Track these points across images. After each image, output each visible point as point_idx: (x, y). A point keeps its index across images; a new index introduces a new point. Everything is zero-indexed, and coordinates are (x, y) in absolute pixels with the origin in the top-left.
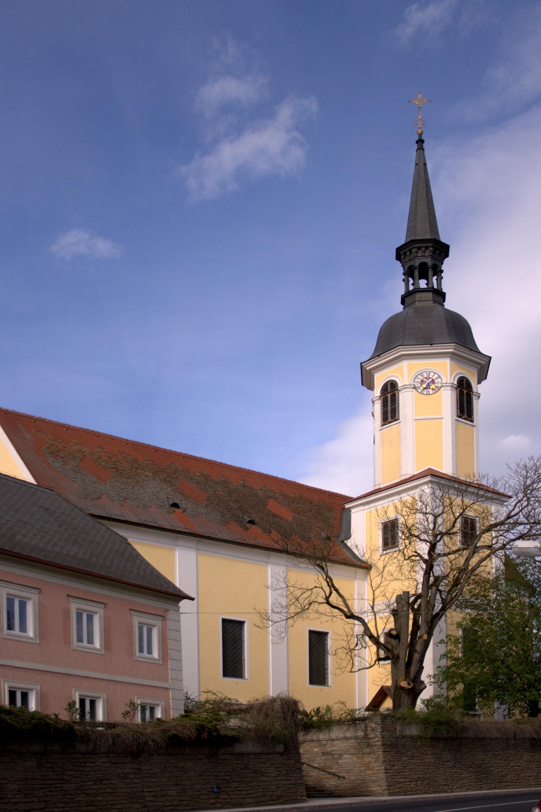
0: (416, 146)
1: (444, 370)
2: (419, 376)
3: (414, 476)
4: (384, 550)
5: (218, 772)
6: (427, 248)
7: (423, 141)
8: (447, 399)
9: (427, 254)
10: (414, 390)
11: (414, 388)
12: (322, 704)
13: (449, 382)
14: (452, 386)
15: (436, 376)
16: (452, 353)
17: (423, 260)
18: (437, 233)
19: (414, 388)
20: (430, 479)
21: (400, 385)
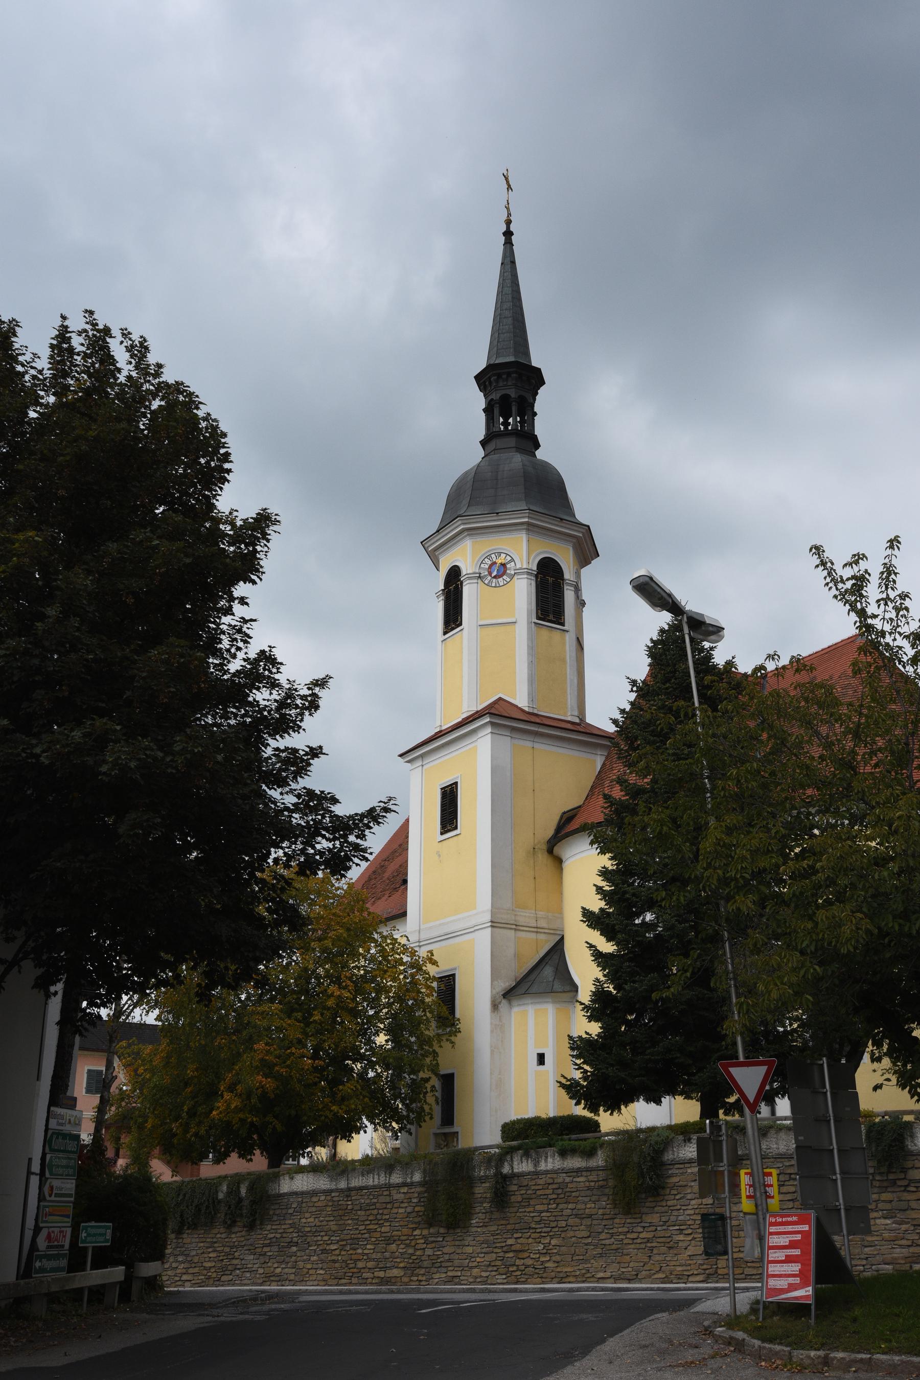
0: (502, 239)
1: (521, 551)
2: (493, 556)
3: (477, 712)
4: (442, 834)
5: (332, 1191)
6: (509, 374)
7: (512, 234)
8: (521, 593)
9: (510, 383)
10: (479, 581)
11: (480, 577)
12: (591, 931)
13: (525, 566)
14: (528, 573)
15: (509, 558)
16: (528, 524)
17: (504, 392)
18: (527, 354)
19: (480, 577)
20: (488, 720)
21: (464, 572)
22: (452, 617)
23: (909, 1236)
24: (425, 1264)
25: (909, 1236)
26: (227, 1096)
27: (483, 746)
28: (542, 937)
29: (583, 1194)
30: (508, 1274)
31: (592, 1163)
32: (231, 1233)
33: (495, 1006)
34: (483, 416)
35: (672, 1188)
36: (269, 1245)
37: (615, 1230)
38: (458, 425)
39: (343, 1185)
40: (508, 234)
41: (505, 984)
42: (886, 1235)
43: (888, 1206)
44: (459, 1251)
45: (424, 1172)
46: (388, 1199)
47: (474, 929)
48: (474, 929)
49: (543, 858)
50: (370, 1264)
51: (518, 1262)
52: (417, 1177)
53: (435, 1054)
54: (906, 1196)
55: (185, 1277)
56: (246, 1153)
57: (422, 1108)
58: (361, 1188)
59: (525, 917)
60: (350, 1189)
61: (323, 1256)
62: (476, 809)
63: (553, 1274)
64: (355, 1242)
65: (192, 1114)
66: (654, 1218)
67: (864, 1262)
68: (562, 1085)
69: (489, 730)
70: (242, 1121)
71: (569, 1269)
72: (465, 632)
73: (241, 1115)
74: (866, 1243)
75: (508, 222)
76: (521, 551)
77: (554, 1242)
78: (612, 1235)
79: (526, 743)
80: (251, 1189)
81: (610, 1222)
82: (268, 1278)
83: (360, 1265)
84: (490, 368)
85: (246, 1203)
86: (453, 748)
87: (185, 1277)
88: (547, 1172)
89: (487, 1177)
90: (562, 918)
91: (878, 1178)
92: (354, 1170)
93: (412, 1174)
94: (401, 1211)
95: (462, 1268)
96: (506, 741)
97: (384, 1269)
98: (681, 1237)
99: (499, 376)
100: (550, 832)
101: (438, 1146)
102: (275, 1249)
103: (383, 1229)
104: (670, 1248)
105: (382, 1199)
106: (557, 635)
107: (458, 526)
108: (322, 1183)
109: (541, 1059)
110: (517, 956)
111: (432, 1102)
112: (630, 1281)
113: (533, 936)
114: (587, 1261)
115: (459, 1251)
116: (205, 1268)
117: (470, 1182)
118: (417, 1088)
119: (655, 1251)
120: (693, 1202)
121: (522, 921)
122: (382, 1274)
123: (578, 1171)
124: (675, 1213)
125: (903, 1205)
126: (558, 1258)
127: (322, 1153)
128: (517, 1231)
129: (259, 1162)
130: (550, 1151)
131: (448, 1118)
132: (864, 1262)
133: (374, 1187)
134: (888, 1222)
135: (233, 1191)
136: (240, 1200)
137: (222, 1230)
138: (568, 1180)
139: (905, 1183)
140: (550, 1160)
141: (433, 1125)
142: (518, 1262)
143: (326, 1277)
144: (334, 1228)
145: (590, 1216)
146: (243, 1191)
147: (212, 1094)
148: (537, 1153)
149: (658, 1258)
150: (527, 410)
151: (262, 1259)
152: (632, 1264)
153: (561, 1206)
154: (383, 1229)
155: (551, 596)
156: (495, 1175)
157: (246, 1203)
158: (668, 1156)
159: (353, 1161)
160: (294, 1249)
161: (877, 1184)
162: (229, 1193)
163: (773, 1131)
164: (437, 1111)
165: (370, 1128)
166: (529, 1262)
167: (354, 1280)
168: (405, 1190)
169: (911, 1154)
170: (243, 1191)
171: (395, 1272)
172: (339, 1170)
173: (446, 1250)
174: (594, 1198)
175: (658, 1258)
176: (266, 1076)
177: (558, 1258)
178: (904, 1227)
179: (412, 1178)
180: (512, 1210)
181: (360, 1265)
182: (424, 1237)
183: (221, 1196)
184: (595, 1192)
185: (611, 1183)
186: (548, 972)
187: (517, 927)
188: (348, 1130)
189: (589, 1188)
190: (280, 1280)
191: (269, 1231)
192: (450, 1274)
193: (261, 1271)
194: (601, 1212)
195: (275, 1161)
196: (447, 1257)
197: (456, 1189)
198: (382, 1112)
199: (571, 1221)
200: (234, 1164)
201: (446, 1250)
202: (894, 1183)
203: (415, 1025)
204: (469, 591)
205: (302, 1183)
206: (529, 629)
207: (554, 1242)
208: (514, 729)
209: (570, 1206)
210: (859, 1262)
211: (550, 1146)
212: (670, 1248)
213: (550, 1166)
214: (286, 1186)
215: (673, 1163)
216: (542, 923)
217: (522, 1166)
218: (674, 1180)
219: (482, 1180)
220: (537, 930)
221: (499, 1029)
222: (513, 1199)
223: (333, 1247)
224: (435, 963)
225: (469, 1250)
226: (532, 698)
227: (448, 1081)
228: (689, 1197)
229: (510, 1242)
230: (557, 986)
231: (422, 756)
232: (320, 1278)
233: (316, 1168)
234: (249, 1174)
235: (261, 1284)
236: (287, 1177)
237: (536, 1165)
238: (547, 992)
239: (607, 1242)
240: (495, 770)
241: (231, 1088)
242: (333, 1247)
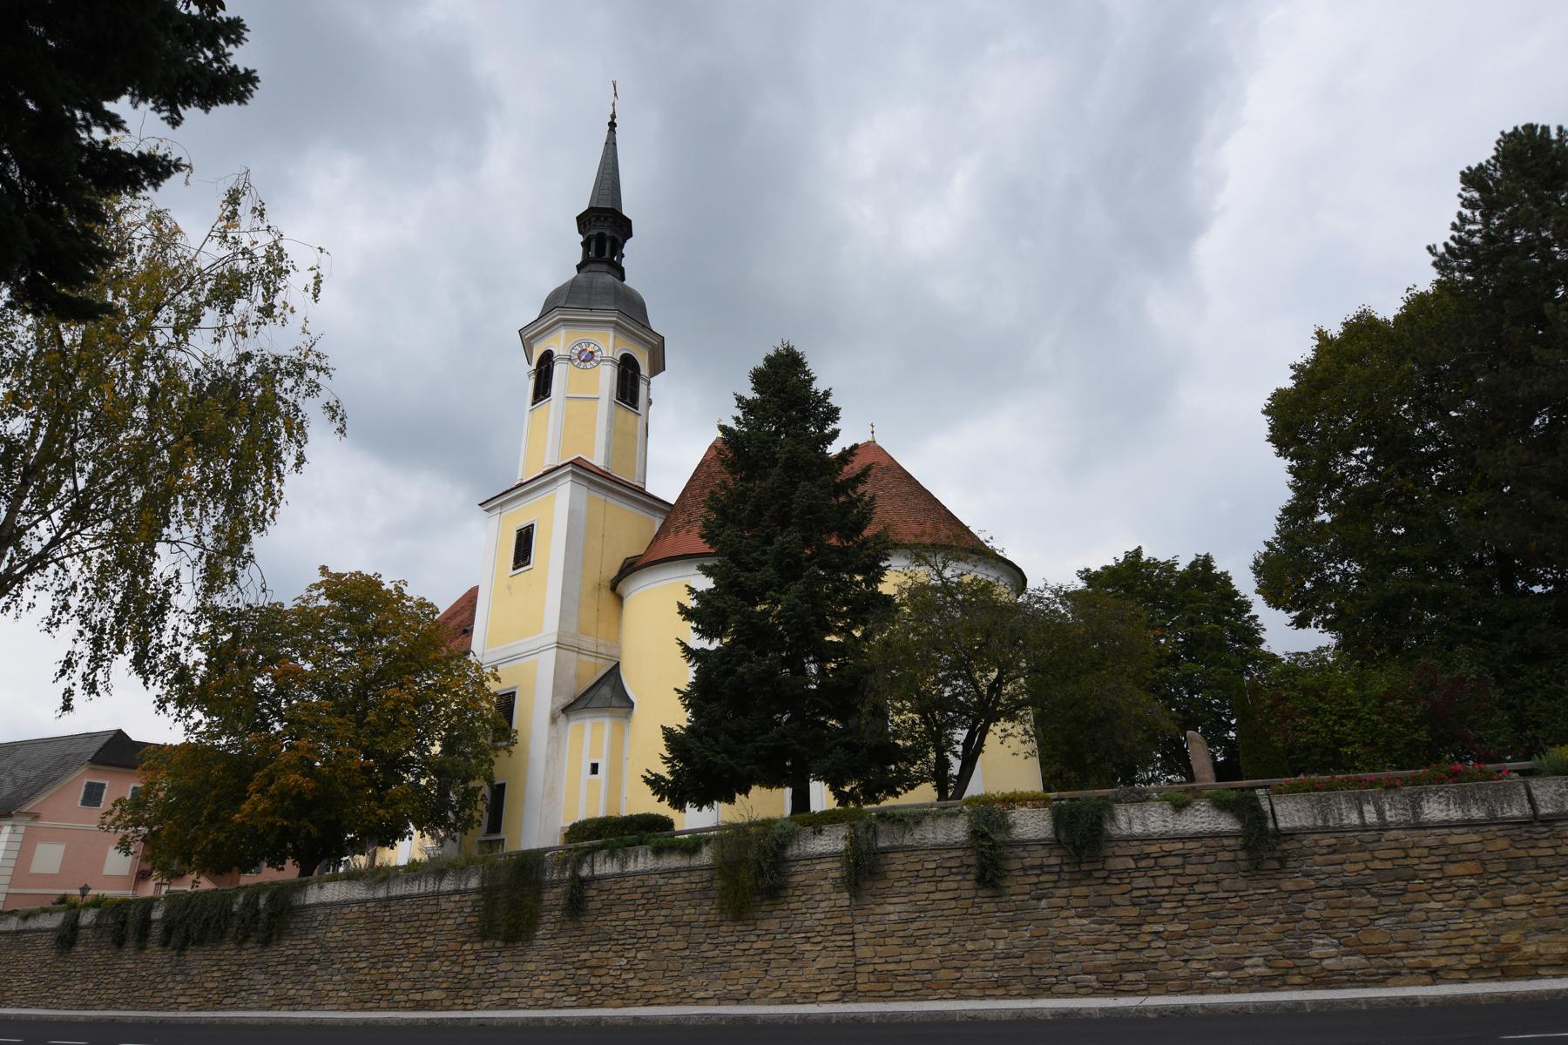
0: (572, 247)
1: (608, 344)
5: (367, 901)
8: (606, 377)
16: (617, 323)
22: (542, 389)
23: (1115, 939)
24: (475, 984)
25: (1115, 939)
26: (255, 797)
27: (564, 493)
28: (600, 661)
29: (680, 897)
30: (579, 995)
31: (696, 861)
32: (242, 949)
33: (554, 720)
34: (581, 249)
35: (795, 888)
36: (284, 963)
37: (721, 940)
38: (563, 255)
39: (381, 893)
40: (612, 125)
41: (564, 700)
42: (1084, 938)
43: (1084, 903)
44: (518, 968)
45: (483, 878)
46: (434, 909)
47: (538, 651)
48: (538, 651)
49: (606, 593)
50: (405, 985)
51: (593, 981)
52: (474, 883)
53: (492, 762)
54: (1106, 890)
55: (181, 999)
56: (277, 862)
57: (471, 816)
58: (403, 897)
59: (588, 643)
60: (389, 899)
61: (347, 976)
62: (551, 550)
63: (638, 995)
64: (389, 959)
65: (212, 819)
66: (773, 925)
67: (1056, 972)
68: (647, 781)
69: (569, 478)
70: (272, 825)
71: (659, 988)
72: (553, 403)
73: (269, 819)
74: (1056, 949)
75: (613, 116)
76: (608, 344)
77: (640, 955)
78: (717, 946)
79: (600, 496)
80: (271, 900)
81: (714, 930)
82: (278, 1003)
83: (392, 985)
84: (591, 210)
85: (263, 916)
86: (531, 497)
87: (181, 999)
88: (635, 874)
89: (561, 881)
90: (620, 647)
91: (1066, 868)
92: (397, 876)
93: (468, 879)
94: (449, 922)
95: (521, 988)
96: (583, 491)
97: (422, 990)
98: (808, 947)
99: (598, 218)
100: (614, 573)
101: (481, 852)
102: (292, 967)
103: (426, 944)
104: (793, 960)
105: (427, 909)
106: (631, 416)
107: (556, 316)
108: (357, 892)
109: (595, 769)
110: (578, 676)
111: (481, 811)
112: (738, 1001)
113: (593, 660)
114: (683, 978)
115: (518, 968)
116: (206, 989)
117: (538, 887)
118: (469, 797)
119: (773, 964)
120: (823, 904)
121: (584, 646)
122: (418, 997)
123: (675, 872)
124: (800, 918)
125: (1103, 901)
126: (645, 975)
127: (361, 861)
128: (594, 943)
129: (291, 871)
130: (641, 849)
131: (495, 824)
132: (1056, 972)
133: (419, 896)
134: (1084, 921)
135: (251, 902)
136: (258, 912)
137: (232, 946)
138: (661, 882)
139: (1105, 874)
140: (640, 859)
141: (478, 833)
142: (593, 981)
143: (349, 1000)
144: (365, 943)
145: (689, 924)
146: (262, 902)
147: (239, 797)
148: (625, 852)
149: (776, 972)
150: (617, 248)
151: (274, 979)
152: (742, 981)
153: (651, 913)
154: (426, 944)
155: (628, 387)
156: (572, 878)
157: (263, 916)
158: (793, 851)
159: (397, 867)
160: (314, 967)
161: (1067, 877)
162: (246, 904)
163: (928, 819)
164: (485, 822)
165: (417, 834)
166: (608, 980)
167: (383, 1004)
168: (457, 898)
169: (1110, 839)
170: (262, 902)
171: (435, 994)
172: (378, 877)
173: (502, 967)
174: (694, 902)
175: (776, 972)
176: (304, 775)
177: (645, 975)
178: (1107, 927)
179: (592, 867)
180: (589, 918)
181: (392, 985)
182: (475, 952)
183: (235, 908)
184: (696, 895)
185: (718, 884)
186: (605, 691)
187: (579, 650)
188: (391, 835)
189: (688, 891)
190: (293, 1004)
191: (287, 947)
192: (505, 996)
193: (271, 993)
194: (703, 918)
195: (306, 871)
196: (502, 975)
197: (520, 899)
198: (431, 818)
199: (663, 930)
200: (267, 874)
201: (502, 967)
202: (1089, 874)
203: (472, 735)
204: (559, 371)
205: (333, 892)
206: (610, 407)
207: (640, 955)
208: (591, 482)
209: (663, 912)
210: (1050, 972)
211: (641, 844)
212: (793, 960)
213: (640, 867)
214: (313, 896)
215: (798, 859)
216: (602, 650)
217: (605, 867)
218: (798, 878)
219: (553, 884)
220: (597, 655)
221: (556, 741)
222: (591, 905)
223: (361, 965)
224: (498, 679)
225: (532, 966)
226: (607, 460)
227: (499, 791)
228: (818, 898)
229: (584, 956)
230: (615, 702)
231: (501, 505)
232: (341, 1001)
233: (353, 876)
234: (272, 883)
235: (269, 1009)
236: (315, 887)
237: (623, 864)
238: (604, 707)
239: (710, 954)
240: (572, 513)
241: (261, 790)
242: (361, 965)
